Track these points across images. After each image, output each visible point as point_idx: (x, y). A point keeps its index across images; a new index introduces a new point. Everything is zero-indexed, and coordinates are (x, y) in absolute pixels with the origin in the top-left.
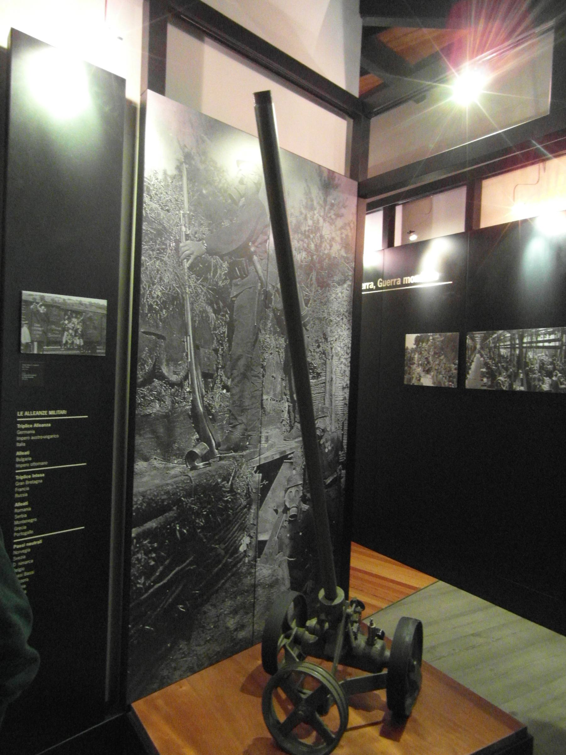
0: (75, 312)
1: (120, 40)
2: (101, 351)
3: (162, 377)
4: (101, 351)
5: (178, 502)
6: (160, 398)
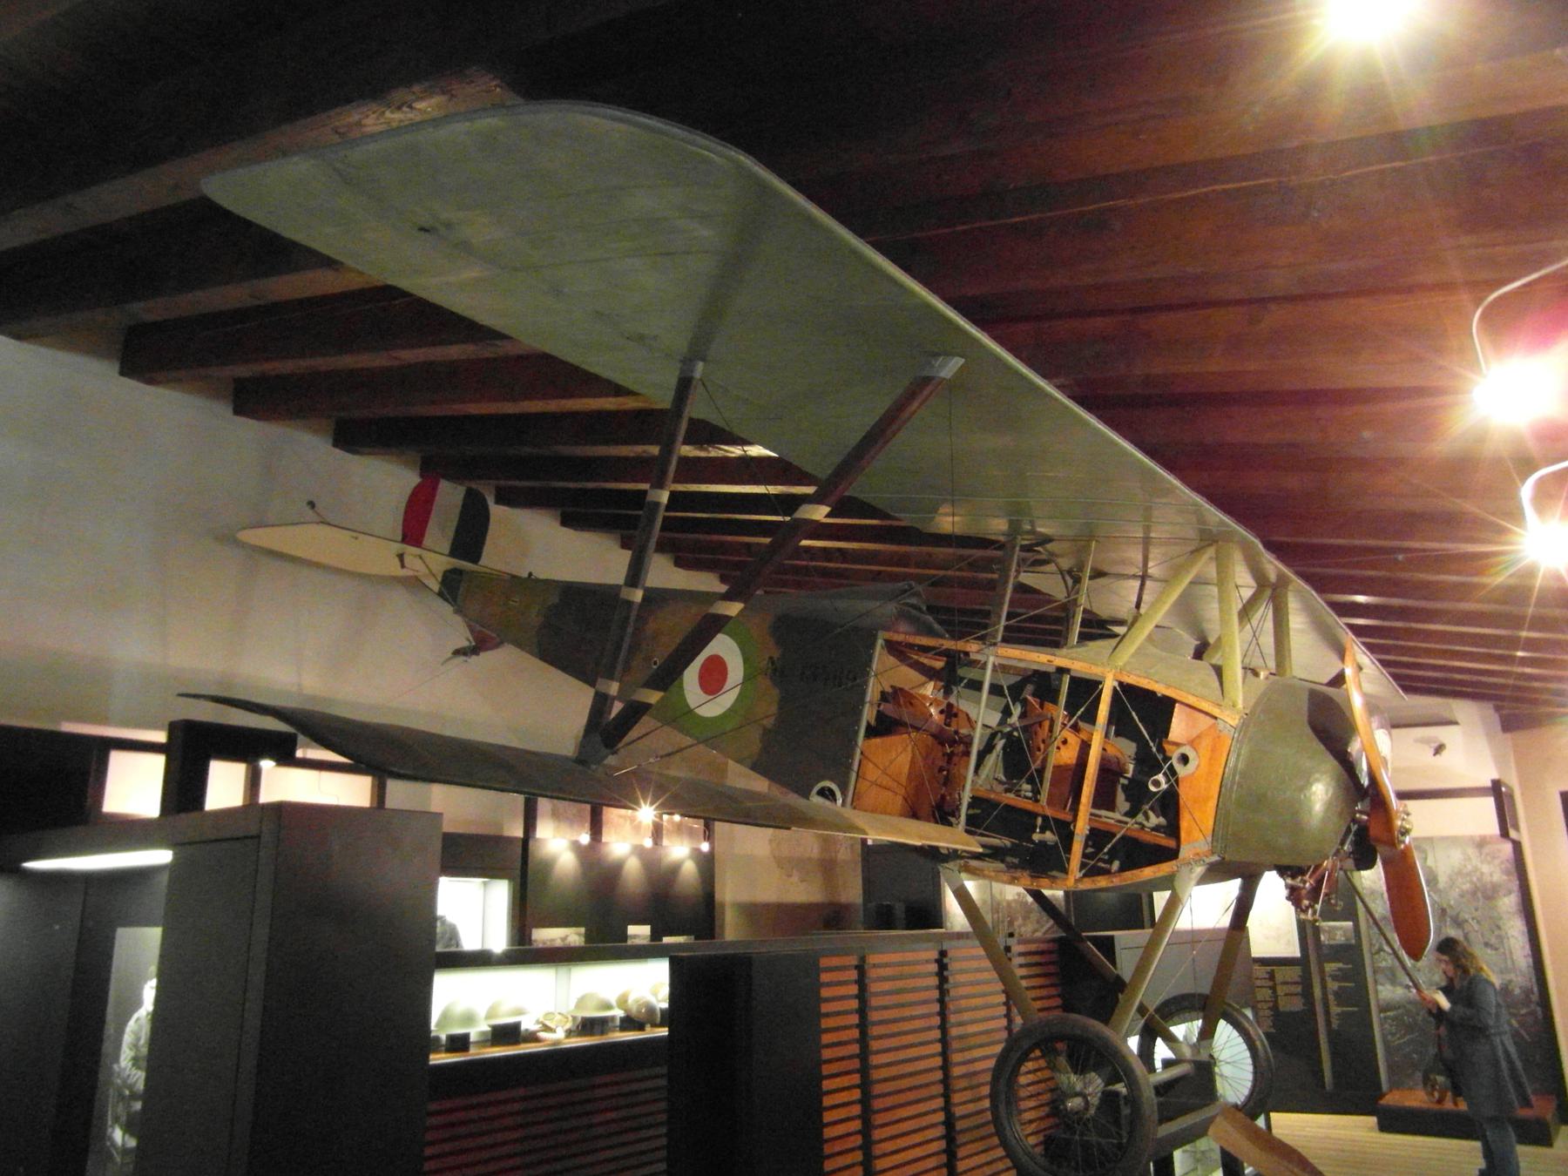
0: (1341, 928)
1: (1445, 753)
2: (1353, 942)
3: (1384, 951)
4: (1353, 942)
5: (1405, 1007)
6: (1385, 960)
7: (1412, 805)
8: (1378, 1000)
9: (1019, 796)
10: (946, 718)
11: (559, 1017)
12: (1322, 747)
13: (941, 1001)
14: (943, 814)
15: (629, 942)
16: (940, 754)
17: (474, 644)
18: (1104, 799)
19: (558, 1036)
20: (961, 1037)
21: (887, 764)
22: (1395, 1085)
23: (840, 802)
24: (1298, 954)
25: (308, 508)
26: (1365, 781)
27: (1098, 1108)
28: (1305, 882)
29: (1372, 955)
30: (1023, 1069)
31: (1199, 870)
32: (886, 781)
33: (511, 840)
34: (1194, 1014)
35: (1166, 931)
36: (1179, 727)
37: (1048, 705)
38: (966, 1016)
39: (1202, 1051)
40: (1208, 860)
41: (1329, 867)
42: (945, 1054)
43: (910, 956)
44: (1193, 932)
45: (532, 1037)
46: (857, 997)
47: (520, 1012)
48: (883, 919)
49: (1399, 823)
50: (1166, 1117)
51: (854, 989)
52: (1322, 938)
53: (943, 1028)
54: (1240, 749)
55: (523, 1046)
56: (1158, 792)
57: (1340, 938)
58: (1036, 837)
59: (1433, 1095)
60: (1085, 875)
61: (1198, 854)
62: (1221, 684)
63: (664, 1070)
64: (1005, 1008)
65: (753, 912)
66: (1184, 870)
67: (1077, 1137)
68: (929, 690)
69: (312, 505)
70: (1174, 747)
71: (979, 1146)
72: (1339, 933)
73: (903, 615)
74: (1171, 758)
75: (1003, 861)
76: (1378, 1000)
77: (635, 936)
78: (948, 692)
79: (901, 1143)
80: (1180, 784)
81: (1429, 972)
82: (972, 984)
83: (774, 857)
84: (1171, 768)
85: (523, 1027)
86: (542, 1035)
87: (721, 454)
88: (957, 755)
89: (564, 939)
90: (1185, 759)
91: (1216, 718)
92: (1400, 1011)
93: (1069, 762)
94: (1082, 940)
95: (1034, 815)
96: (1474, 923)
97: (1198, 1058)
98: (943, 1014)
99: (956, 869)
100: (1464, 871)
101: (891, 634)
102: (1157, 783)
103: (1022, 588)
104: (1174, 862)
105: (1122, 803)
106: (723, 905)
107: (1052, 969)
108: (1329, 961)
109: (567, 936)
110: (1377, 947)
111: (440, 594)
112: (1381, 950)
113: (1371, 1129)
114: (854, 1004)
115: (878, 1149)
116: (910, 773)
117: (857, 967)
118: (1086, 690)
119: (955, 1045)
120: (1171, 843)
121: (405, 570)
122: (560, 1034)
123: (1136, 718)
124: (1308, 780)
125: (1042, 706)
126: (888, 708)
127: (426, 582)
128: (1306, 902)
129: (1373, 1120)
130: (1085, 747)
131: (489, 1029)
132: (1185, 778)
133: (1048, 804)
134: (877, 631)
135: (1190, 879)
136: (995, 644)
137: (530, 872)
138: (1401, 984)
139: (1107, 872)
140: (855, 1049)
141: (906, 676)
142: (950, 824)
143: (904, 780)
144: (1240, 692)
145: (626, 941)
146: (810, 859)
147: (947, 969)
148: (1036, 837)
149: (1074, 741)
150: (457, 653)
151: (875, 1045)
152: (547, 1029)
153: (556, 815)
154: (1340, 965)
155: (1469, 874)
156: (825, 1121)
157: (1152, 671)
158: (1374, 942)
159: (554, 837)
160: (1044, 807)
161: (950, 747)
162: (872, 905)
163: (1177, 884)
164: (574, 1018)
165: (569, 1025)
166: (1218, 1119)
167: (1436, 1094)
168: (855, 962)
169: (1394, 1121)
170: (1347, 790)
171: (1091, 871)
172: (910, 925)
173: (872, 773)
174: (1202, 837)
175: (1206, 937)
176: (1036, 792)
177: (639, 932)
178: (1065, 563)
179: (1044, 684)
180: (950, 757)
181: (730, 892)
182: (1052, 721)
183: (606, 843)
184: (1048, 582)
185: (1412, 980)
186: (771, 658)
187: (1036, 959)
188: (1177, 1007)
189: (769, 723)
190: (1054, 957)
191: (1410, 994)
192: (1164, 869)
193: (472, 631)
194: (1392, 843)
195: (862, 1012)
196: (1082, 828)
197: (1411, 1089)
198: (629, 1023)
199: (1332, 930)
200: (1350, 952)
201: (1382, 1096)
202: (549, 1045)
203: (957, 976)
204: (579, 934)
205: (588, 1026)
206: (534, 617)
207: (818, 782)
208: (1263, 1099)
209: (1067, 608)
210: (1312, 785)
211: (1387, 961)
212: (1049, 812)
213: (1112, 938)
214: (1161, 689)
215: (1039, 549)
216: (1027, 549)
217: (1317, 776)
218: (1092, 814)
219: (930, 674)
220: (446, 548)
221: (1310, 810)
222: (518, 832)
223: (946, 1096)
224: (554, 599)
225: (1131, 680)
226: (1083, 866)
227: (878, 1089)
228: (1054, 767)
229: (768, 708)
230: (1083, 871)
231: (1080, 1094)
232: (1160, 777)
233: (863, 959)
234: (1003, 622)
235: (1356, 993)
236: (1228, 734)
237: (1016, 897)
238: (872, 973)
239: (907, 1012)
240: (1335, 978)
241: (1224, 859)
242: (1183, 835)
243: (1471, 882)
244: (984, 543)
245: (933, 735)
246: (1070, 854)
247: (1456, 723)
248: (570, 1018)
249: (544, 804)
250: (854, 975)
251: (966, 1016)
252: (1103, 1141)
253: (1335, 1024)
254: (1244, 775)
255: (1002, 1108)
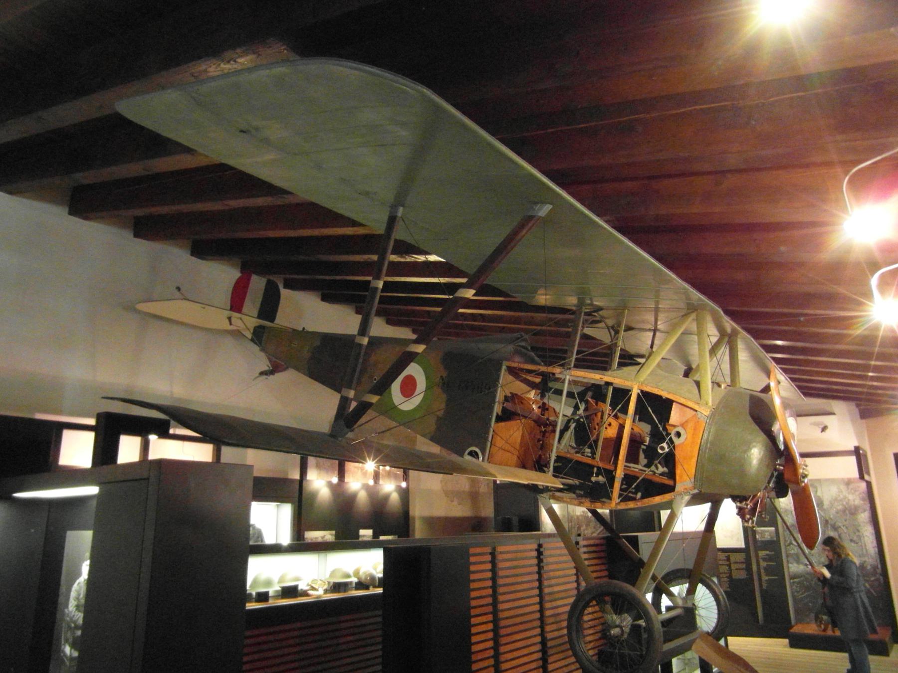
0: (768, 531)
1: (827, 431)
2: (775, 539)
3: (793, 544)
4: (775, 539)
5: (804, 576)
6: (793, 549)
7: (809, 461)
8: (789, 573)
9: (584, 456)
10: (542, 411)
11: (320, 582)
12: (757, 428)
13: (539, 573)
14: (540, 466)
15: (360, 539)
16: (539, 431)
17: (271, 368)
18: (632, 457)
19: (320, 593)
20: (550, 594)
21: (508, 437)
22: (799, 621)
23: (481, 459)
24: (743, 546)
25: (176, 291)
26: (782, 447)
27: (629, 634)
28: (747, 505)
29: (786, 546)
30: (586, 612)
31: (687, 498)
32: (507, 447)
33: (292, 481)
34: (684, 580)
35: (668, 533)
36: (675, 416)
37: (600, 404)
38: (553, 582)
39: (688, 601)
40: (692, 492)
41: (761, 496)
42: (541, 603)
43: (521, 547)
44: (683, 534)
45: (305, 594)
46: (491, 570)
47: (298, 579)
48: (506, 526)
49: (801, 471)
50: (668, 639)
51: (489, 566)
52: (757, 537)
53: (540, 588)
54: (710, 429)
55: (299, 598)
56: (663, 453)
57: (767, 537)
58: (593, 479)
59: (821, 627)
60: (621, 501)
61: (686, 489)
62: (699, 391)
63: (380, 612)
64: (575, 577)
65: (431, 522)
66: (678, 498)
67: (617, 651)
68: (532, 395)
69: (179, 289)
70: (673, 428)
71: (561, 656)
72: (767, 534)
73: (517, 352)
74: (670, 434)
75: (574, 493)
76: (789, 573)
77: (364, 536)
78: (543, 396)
79: (516, 654)
80: (676, 448)
81: (819, 556)
82: (557, 563)
83: (444, 490)
84: (671, 440)
85: (300, 588)
86: (311, 592)
87: (413, 260)
88: (548, 432)
89: (323, 537)
90: (678, 435)
91: (696, 411)
92: (802, 579)
93: (612, 436)
94: (620, 538)
95: (592, 467)
96: (844, 528)
97: (686, 606)
98: (540, 580)
99: (547, 497)
100: (839, 499)
101: (510, 363)
102: (662, 448)
103: (585, 337)
104: (672, 493)
105: (643, 460)
106: (414, 518)
107: (603, 554)
108: (761, 550)
109: (325, 536)
110: (788, 542)
111: (252, 340)
112: (791, 543)
113: (785, 646)
114: (489, 575)
115: (503, 658)
116: (521, 443)
117: (491, 553)
118: (622, 395)
119: (547, 598)
120: (671, 483)
121: (232, 326)
122: (320, 592)
123: (651, 411)
124: (749, 447)
125: (597, 404)
126: (509, 405)
127: (244, 333)
128: (748, 516)
129: (786, 641)
130: (621, 427)
131: (280, 589)
132: (679, 445)
133: (600, 460)
134: (502, 361)
135: (682, 503)
136: (570, 369)
137: (303, 499)
138: (802, 563)
139: (634, 499)
140: (490, 600)
141: (519, 387)
142: (544, 472)
143: (517, 446)
144: (710, 396)
145: (358, 539)
146: (464, 492)
147: (542, 555)
148: (593, 479)
149: (615, 424)
150: (262, 373)
151: (501, 598)
152: (313, 589)
153: (318, 467)
154: (768, 552)
155: (841, 500)
156: (473, 641)
157: (660, 384)
158: (787, 539)
159: (317, 479)
160: (598, 462)
161: (544, 427)
162: (500, 518)
163: (674, 506)
164: (329, 583)
165: (326, 587)
166: (698, 641)
167: (823, 626)
168: (490, 551)
169: (798, 642)
170: (771, 452)
171: (625, 499)
172: (521, 530)
173: (499, 442)
174: (688, 479)
175: (691, 536)
176: (593, 453)
177: (366, 534)
178: (610, 322)
179: (598, 391)
180: (544, 433)
181: (418, 511)
182: (603, 413)
183: (347, 483)
184: (600, 333)
185: (808, 561)
186: (441, 377)
187: (593, 549)
188: (674, 576)
189: (440, 414)
190: (604, 548)
191: (808, 569)
192: (667, 497)
193: (270, 361)
194: (797, 482)
195: (494, 579)
196: (619, 474)
197: (808, 623)
198: (360, 585)
199: (763, 532)
200: (773, 545)
201: (792, 627)
202: (314, 598)
203: (548, 559)
204: (332, 535)
205: (337, 587)
206: (306, 353)
207: (468, 447)
208: (724, 629)
209: (611, 348)
210: (751, 449)
211: (794, 550)
212: (601, 465)
213: (637, 537)
214: (665, 395)
215: (595, 314)
216: (588, 314)
217: (754, 444)
218: (625, 466)
219: (533, 385)
220: (255, 313)
221: (750, 464)
222: (296, 476)
223: (542, 627)
224: (317, 343)
225: (648, 389)
226: (620, 495)
227: (503, 623)
228: (604, 439)
229: (440, 405)
230: (620, 499)
231: (619, 626)
232: (664, 445)
233: (494, 549)
234: (574, 356)
235: (776, 568)
236: (703, 420)
237: (582, 513)
238: (500, 557)
239: (519, 579)
240: (765, 560)
241: (701, 491)
242: (677, 478)
243: (843, 505)
244: (563, 311)
245: (534, 421)
246: (613, 488)
247: (834, 414)
248: (327, 583)
249: (311, 460)
250: (489, 558)
251: (553, 582)
252: (632, 653)
253: (765, 586)
254: (712, 443)
255: (574, 634)
